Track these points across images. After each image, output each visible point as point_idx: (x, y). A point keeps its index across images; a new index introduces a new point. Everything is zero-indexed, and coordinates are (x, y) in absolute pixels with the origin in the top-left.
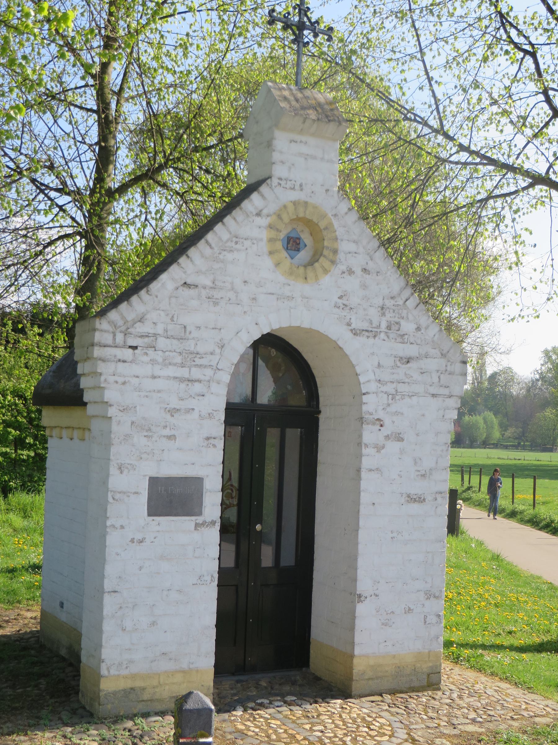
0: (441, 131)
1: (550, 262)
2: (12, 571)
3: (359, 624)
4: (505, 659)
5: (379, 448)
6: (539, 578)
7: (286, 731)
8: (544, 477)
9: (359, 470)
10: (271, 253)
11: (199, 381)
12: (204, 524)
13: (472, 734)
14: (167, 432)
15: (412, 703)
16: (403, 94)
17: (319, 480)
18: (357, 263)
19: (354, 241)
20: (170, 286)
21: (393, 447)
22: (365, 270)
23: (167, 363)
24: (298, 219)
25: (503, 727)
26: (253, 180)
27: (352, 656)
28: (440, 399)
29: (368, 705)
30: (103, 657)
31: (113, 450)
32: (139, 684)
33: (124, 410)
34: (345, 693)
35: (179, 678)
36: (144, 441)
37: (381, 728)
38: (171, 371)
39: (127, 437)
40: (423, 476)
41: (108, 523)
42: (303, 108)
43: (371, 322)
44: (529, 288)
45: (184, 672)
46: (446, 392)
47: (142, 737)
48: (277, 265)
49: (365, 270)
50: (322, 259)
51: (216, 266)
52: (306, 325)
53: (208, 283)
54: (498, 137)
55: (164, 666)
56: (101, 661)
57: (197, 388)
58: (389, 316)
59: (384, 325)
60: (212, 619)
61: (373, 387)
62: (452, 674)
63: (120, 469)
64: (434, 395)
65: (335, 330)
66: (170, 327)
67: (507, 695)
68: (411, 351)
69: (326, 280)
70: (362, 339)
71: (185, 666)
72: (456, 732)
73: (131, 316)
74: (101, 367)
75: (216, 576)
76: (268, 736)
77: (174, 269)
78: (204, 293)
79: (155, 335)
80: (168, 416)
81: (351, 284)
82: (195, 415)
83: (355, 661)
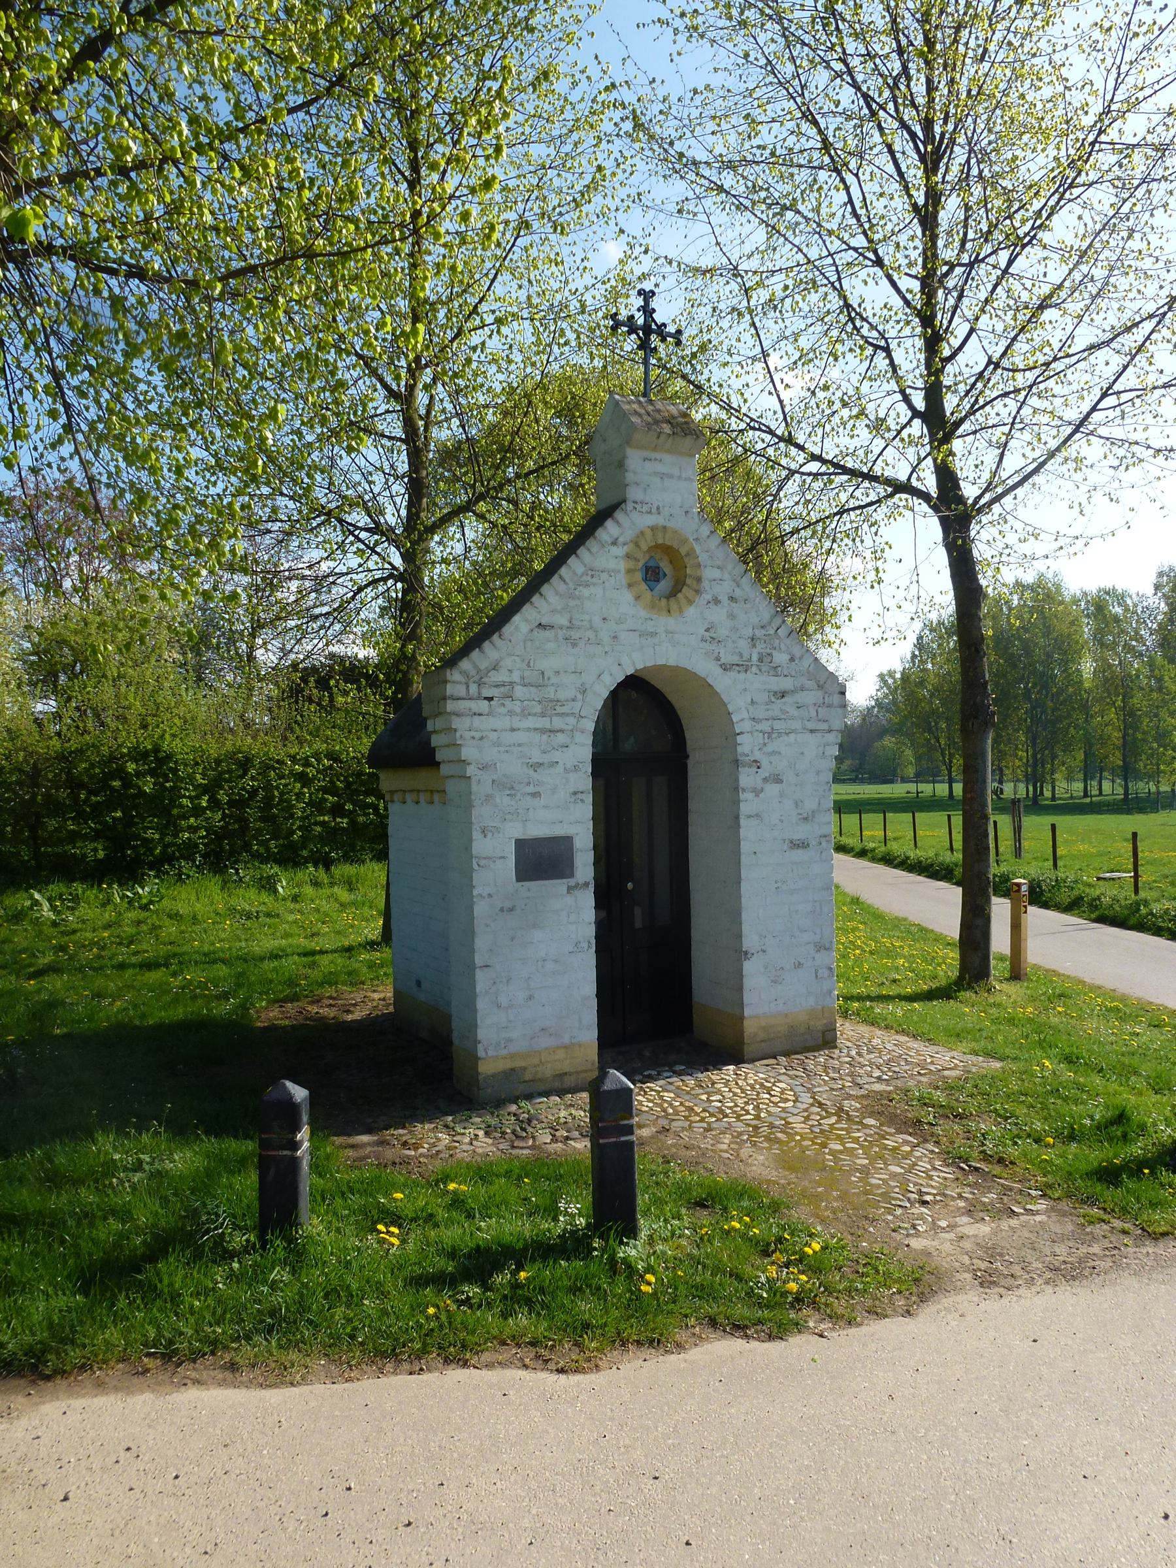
0: (789, 440)
1: (915, 578)
2: (349, 949)
3: (748, 983)
4: (897, 1010)
5: (757, 792)
6: (905, 919)
7: (682, 1104)
8: (868, 812)
9: (737, 817)
10: (630, 585)
11: (562, 731)
12: (577, 886)
13: (880, 1093)
14: (531, 789)
15: (811, 1065)
16: (745, 401)
17: (692, 830)
18: (723, 590)
19: (717, 566)
20: (524, 628)
21: (772, 790)
22: (732, 598)
23: (525, 713)
24: (657, 547)
25: (911, 1083)
26: (603, 506)
27: (741, 1018)
28: (819, 735)
29: (764, 1069)
30: (479, 1037)
31: (475, 812)
32: (519, 1063)
33: (484, 768)
34: (737, 1058)
35: (561, 1054)
36: (507, 801)
37: (782, 1092)
38: (531, 722)
39: (489, 797)
40: (806, 819)
41: (475, 893)
42: (656, 422)
43: (741, 655)
44: (893, 608)
45: (565, 1047)
46: (825, 726)
47: (529, 1121)
48: (637, 598)
49: (732, 598)
50: (685, 589)
51: (572, 603)
52: (672, 663)
53: (566, 623)
54: (853, 444)
55: (545, 1042)
56: (476, 1042)
57: (561, 738)
58: (761, 647)
59: (755, 657)
60: (590, 988)
61: (747, 726)
62: (847, 1031)
63: (484, 832)
64: (812, 731)
65: (704, 667)
66: (527, 673)
67: (909, 1049)
68: (786, 684)
69: (691, 612)
70: (732, 674)
71: (566, 1040)
72: (862, 1092)
73: (484, 665)
74: (456, 723)
75: (593, 941)
76: (664, 1110)
77: (527, 610)
78: (561, 633)
79: (511, 683)
80: (531, 772)
81: (718, 615)
82: (560, 769)
83: (746, 1023)
